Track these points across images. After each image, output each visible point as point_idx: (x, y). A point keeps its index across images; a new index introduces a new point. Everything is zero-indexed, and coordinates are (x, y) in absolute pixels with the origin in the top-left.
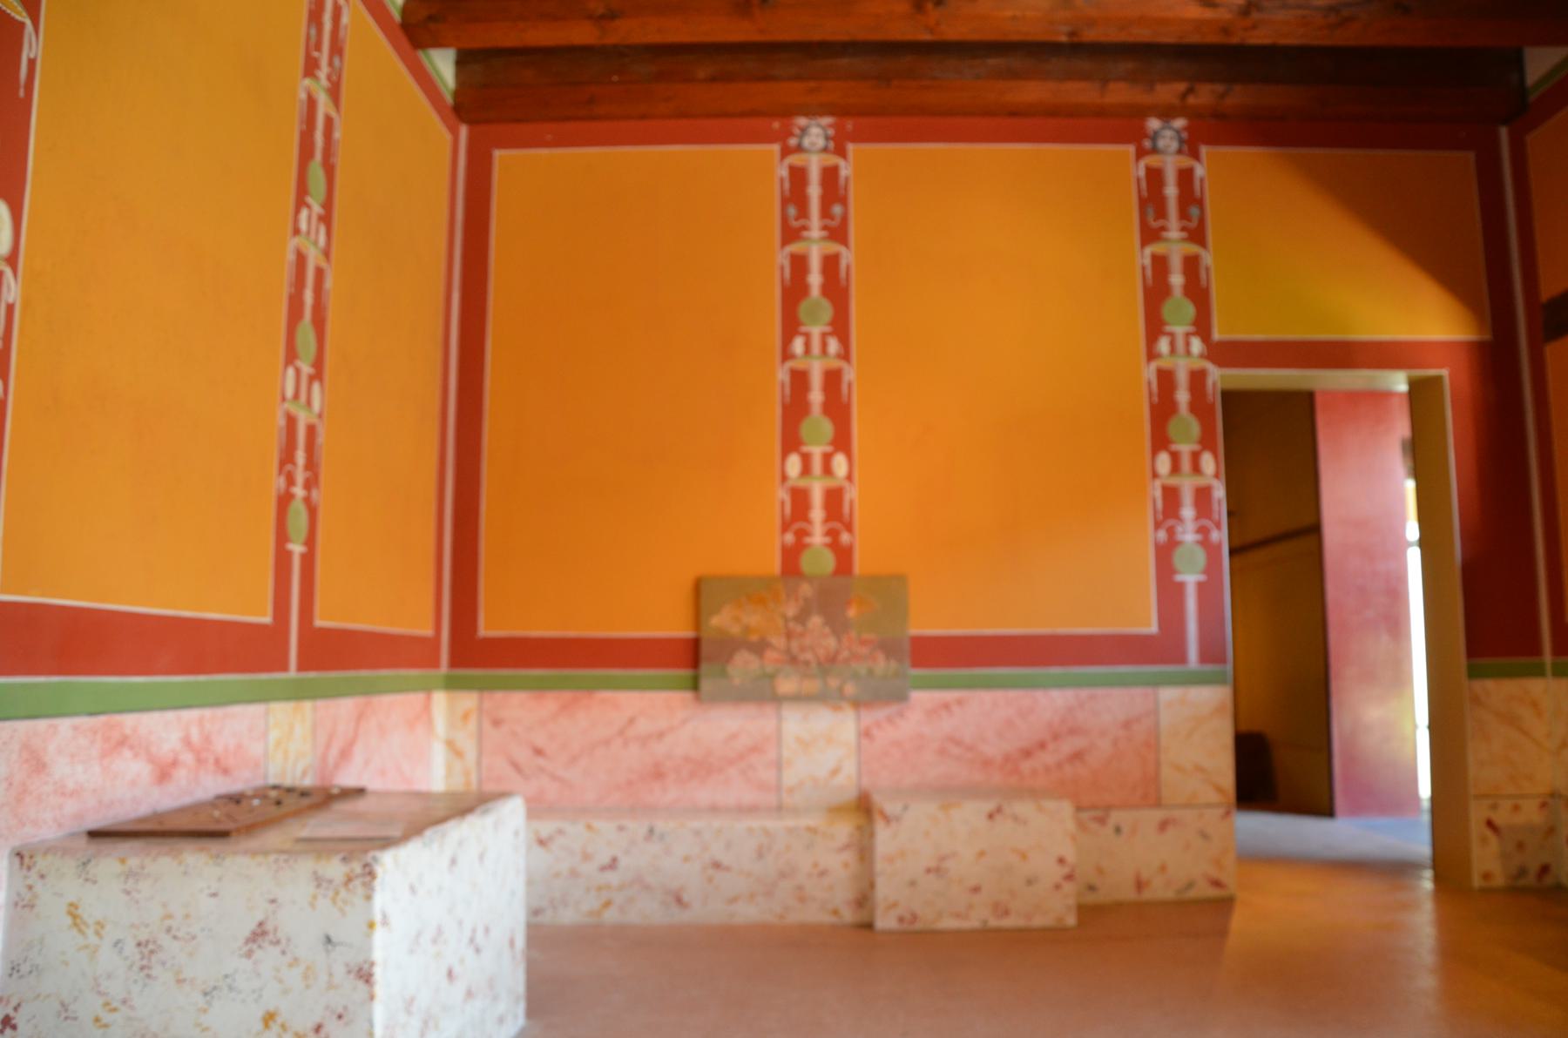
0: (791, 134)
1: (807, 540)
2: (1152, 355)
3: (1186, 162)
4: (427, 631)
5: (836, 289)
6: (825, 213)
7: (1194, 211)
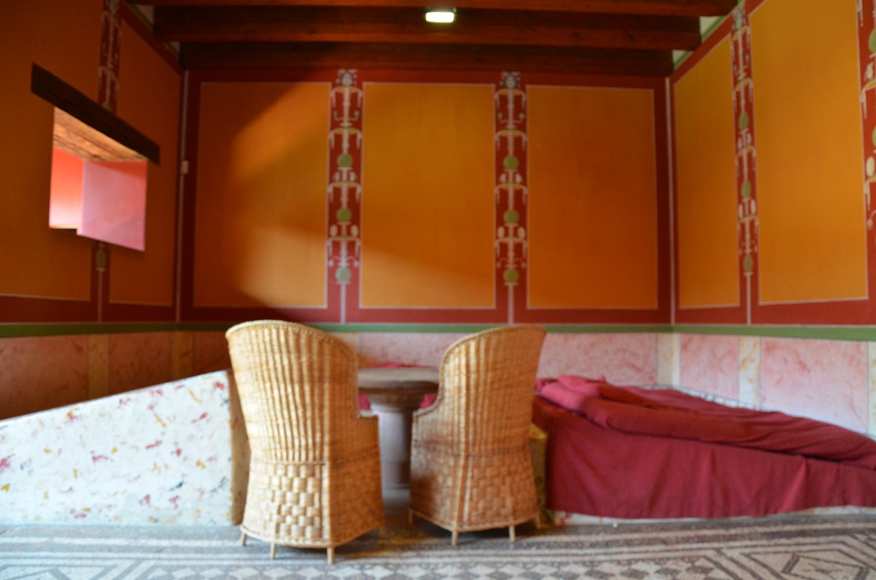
0: (500, 80)
2: (498, 182)
3: (519, 92)
4: (169, 304)
5: (355, 152)
6: (516, 117)
7: (357, 113)
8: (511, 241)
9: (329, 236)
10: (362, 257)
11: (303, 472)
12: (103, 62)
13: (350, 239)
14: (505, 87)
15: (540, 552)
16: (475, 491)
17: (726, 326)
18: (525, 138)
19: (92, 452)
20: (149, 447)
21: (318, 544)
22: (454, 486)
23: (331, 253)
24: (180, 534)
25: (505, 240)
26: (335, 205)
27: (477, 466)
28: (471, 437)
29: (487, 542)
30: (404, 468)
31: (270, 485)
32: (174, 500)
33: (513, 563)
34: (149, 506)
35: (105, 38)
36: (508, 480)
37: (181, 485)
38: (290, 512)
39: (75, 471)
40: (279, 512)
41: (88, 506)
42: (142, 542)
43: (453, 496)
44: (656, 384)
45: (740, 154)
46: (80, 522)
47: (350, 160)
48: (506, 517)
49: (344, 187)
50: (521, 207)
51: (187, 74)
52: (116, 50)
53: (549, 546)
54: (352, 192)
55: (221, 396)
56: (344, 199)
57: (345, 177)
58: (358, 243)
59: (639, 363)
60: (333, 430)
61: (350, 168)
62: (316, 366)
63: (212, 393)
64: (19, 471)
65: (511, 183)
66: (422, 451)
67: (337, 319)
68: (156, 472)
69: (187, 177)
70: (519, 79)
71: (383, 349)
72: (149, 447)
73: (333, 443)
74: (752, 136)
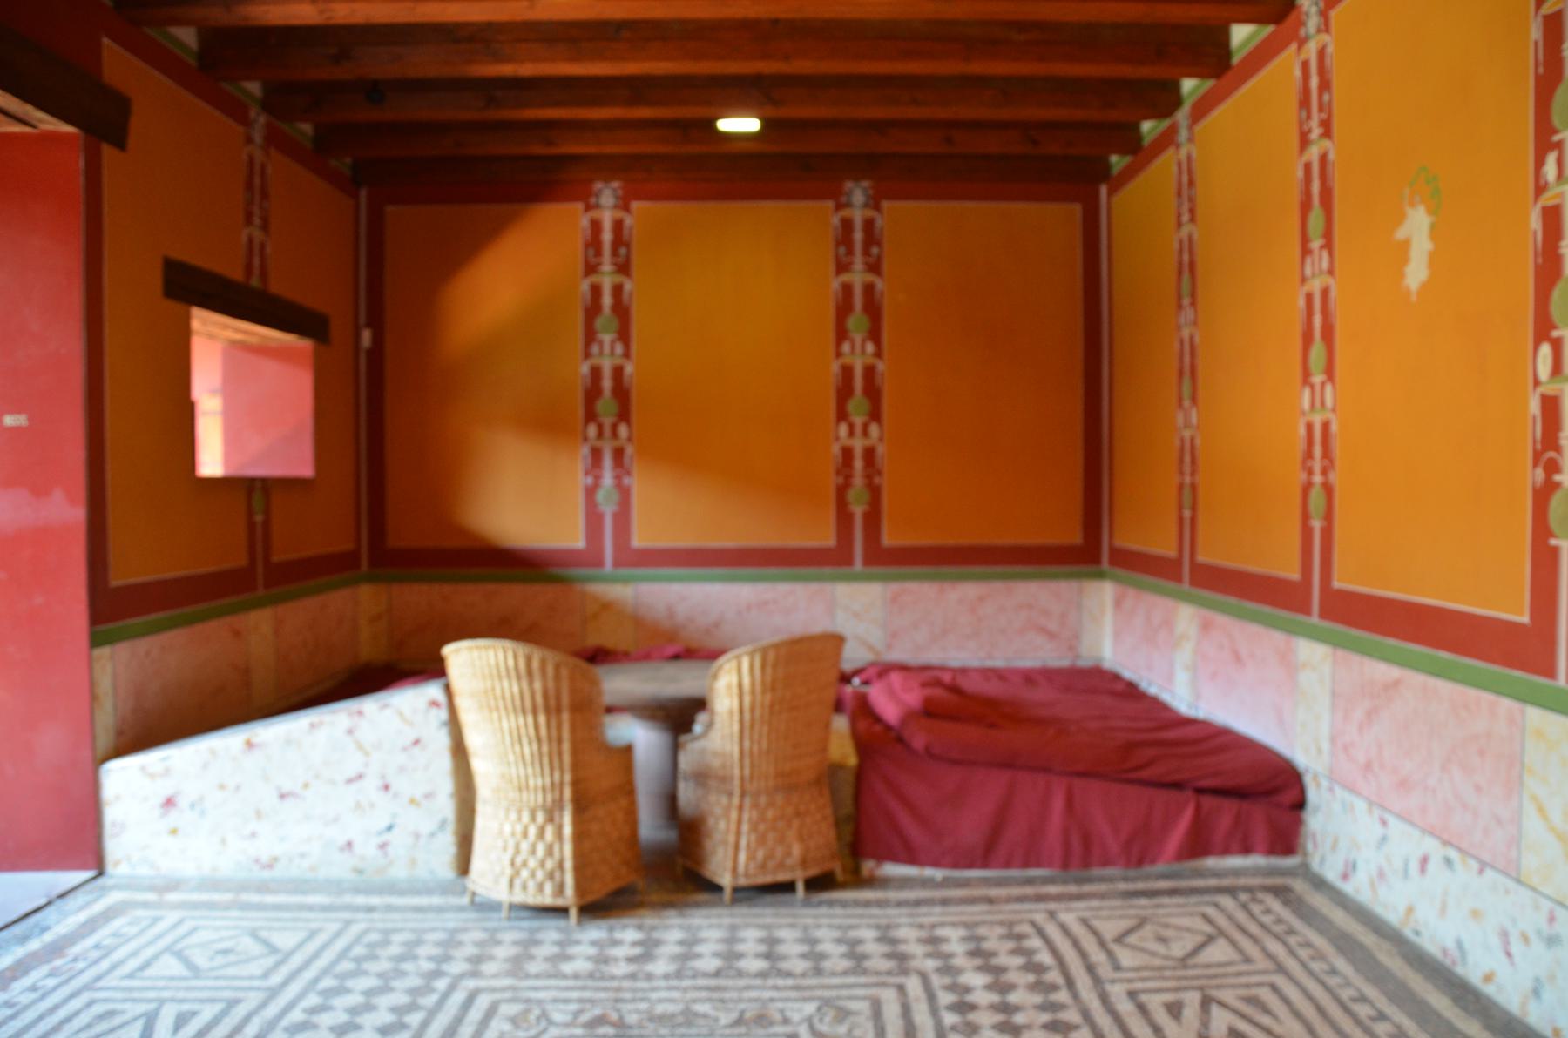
2: (839, 354)
3: (870, 213)
4: (348, 546)
5: (622, 311)
6: (866, 252)
7: (623, 251)
8: (858, 445)
9: (586, 439)
10: (635, 470)
11: (540, 817)
12: (249, 219)
13: (616, 444)
14: (848, 205)
15: (831, 911)
16: (753, 837)
18: (880, 285)
21: (560, 902)
22: (728, 830)
24: (392, 888)
26: (592, 393)
27: (755, 806)
28: (747, 772)
29: (769, 898)
30: (670, 801)
31: (501, 832)
32: (383, 846)
33: (792, 926)
35: (249, 185)
36: (796, 823)
38: (525, 864)
40: (513, 864)
42: (348, 899)
43: (725, 843)
44: (1077, 657)
46: (266, 874)
47: (615, 324)
48: (792, 868)
49: (607, 365)
51: (363, 193)
52: (265, 195)
53: (844, 904)
54: (618, 372)
56: (607, 383)
57: (607, 349)
58: (630, 450)
59: (1053, 626)
60: (575, 766)
65: (859, 354)
66: (691, 784)
67: (599, 563)
69: (370, 352)
72: (350, 781)
73: (575, 783)
74: (1196, 311)
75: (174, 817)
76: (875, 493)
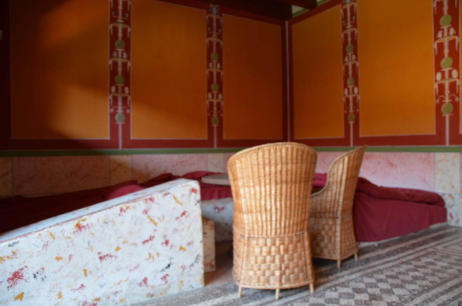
1: (117, 111)
3: (219, 17)
5: (126, 40)
6: (217, 31)
8: (215, 101)
9: (111, 93)
13: (124, 95)
14: (211, 13)
17: (333, 147)
18: (222, 44)
19: (99, 253)
20: (144, 242)
23: (112, 105)
25: (212, 100)
26: (114, 73)
34: (147, 286)
37: (169, 266)
39: (85, 271)
41: (97, 296)
45: (346, 64)
50: (220, 82)
54: (125, 65)
55: (195, 198)
56: (120, 69)
57: (120, 55)
58: (129, 98)
61: (352, 53)
62: (294, 173)
63: (189, 197)
64: (32, 280)
65: (215, 68)
67: (118, 147)
68: (151, 259)
70: (219, 9)
71: (146, 165)
75: (20, 286)
76: (221, 119)
